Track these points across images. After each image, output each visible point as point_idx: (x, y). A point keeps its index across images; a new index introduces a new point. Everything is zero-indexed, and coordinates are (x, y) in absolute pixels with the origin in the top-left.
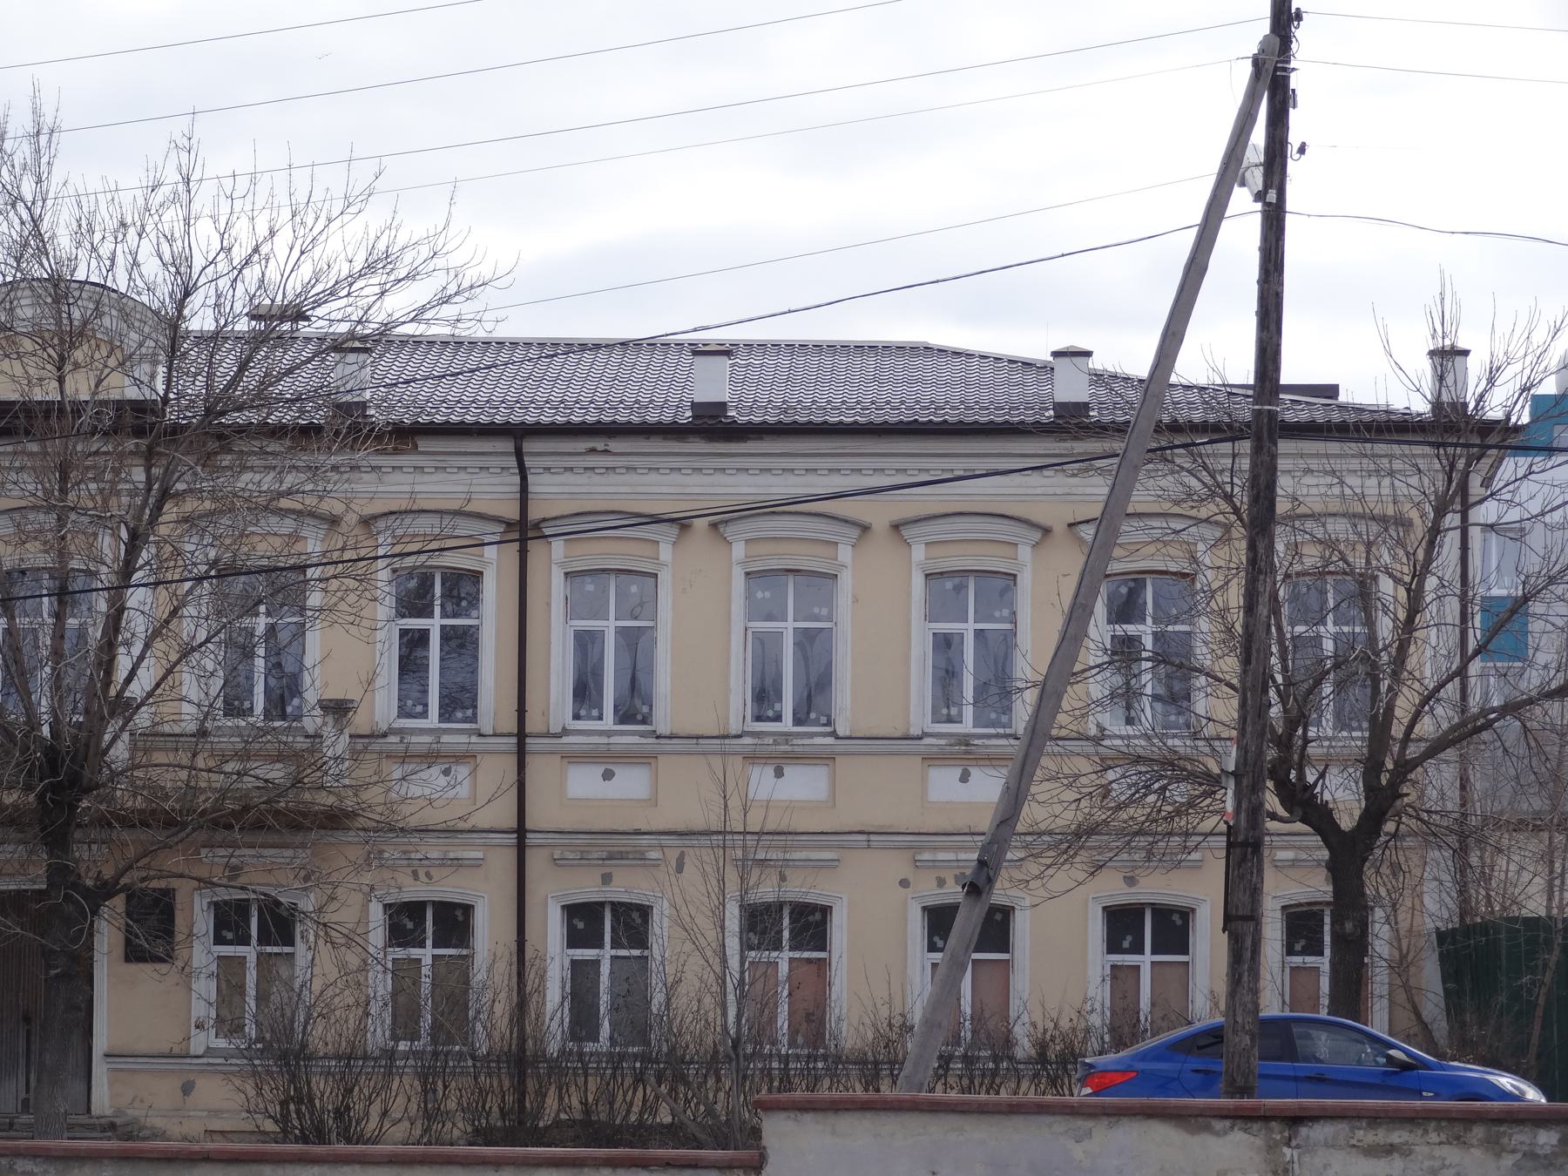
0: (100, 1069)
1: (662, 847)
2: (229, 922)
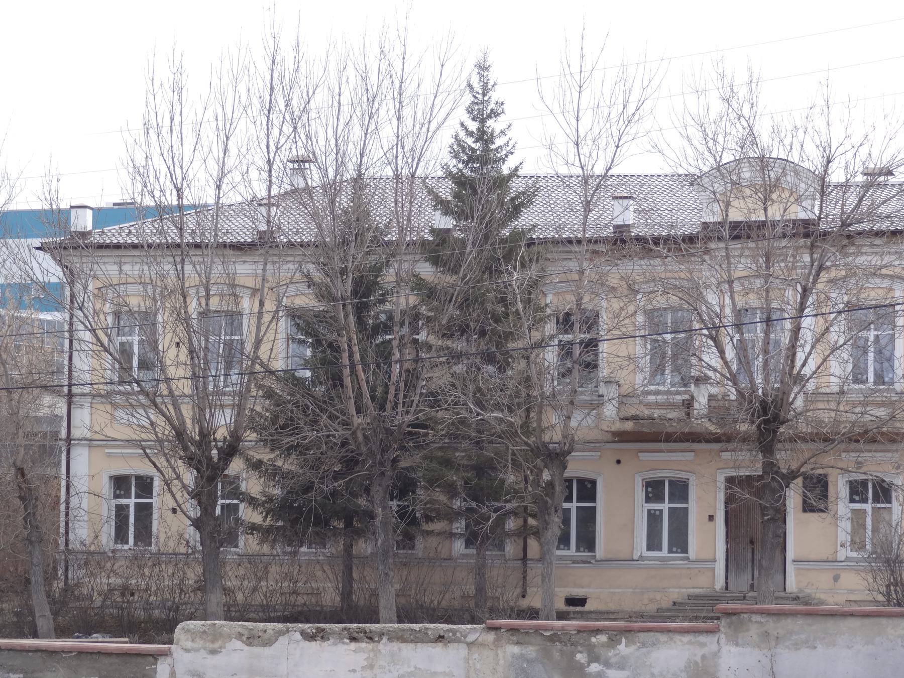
0: (790, 568)
2: (857, 491)
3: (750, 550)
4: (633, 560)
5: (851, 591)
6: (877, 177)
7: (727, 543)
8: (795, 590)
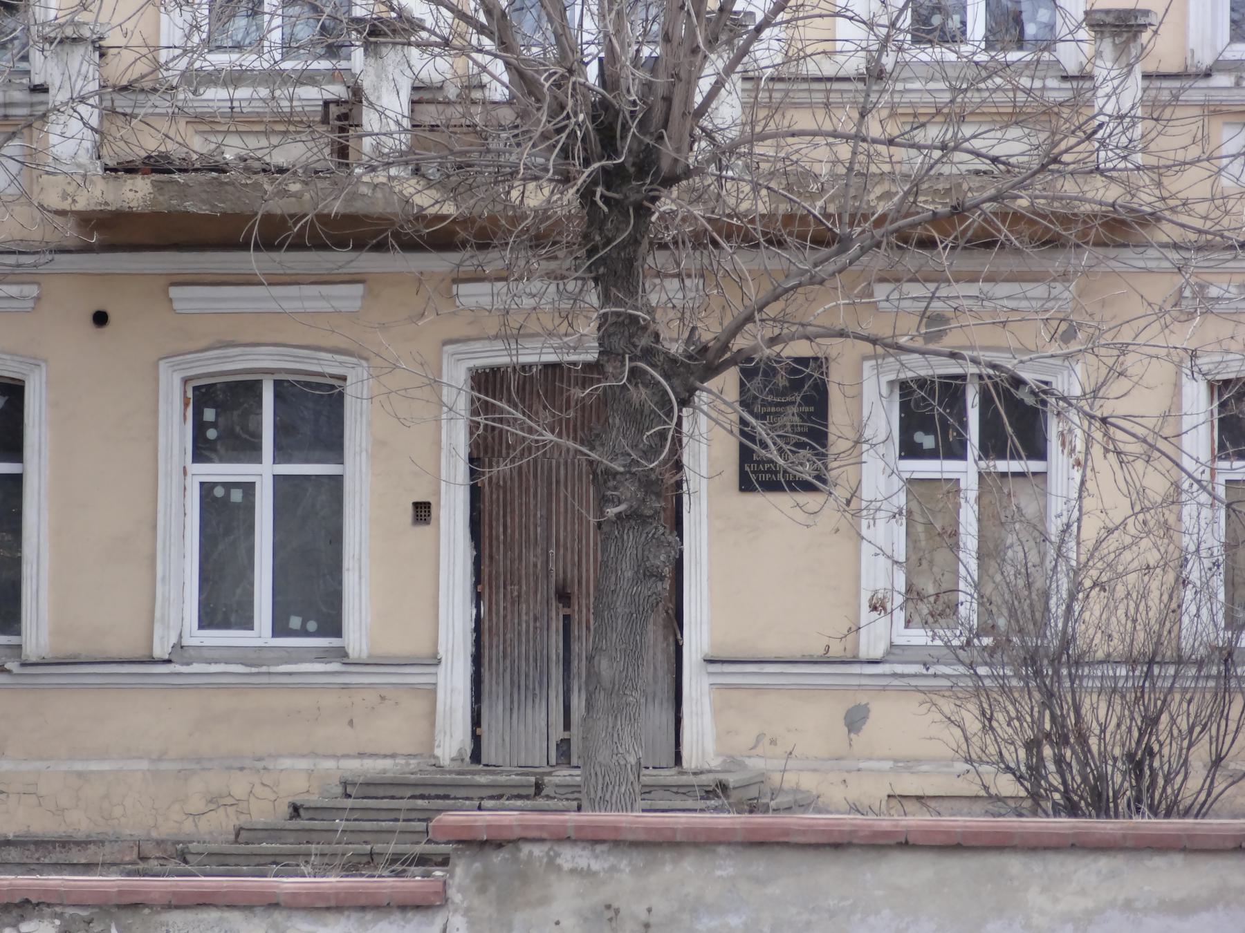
0: (697, 685)
2: (927, 416)
3: (557, 625)
4: (153, 661)
7: (478, 598)
8: (714, 762)
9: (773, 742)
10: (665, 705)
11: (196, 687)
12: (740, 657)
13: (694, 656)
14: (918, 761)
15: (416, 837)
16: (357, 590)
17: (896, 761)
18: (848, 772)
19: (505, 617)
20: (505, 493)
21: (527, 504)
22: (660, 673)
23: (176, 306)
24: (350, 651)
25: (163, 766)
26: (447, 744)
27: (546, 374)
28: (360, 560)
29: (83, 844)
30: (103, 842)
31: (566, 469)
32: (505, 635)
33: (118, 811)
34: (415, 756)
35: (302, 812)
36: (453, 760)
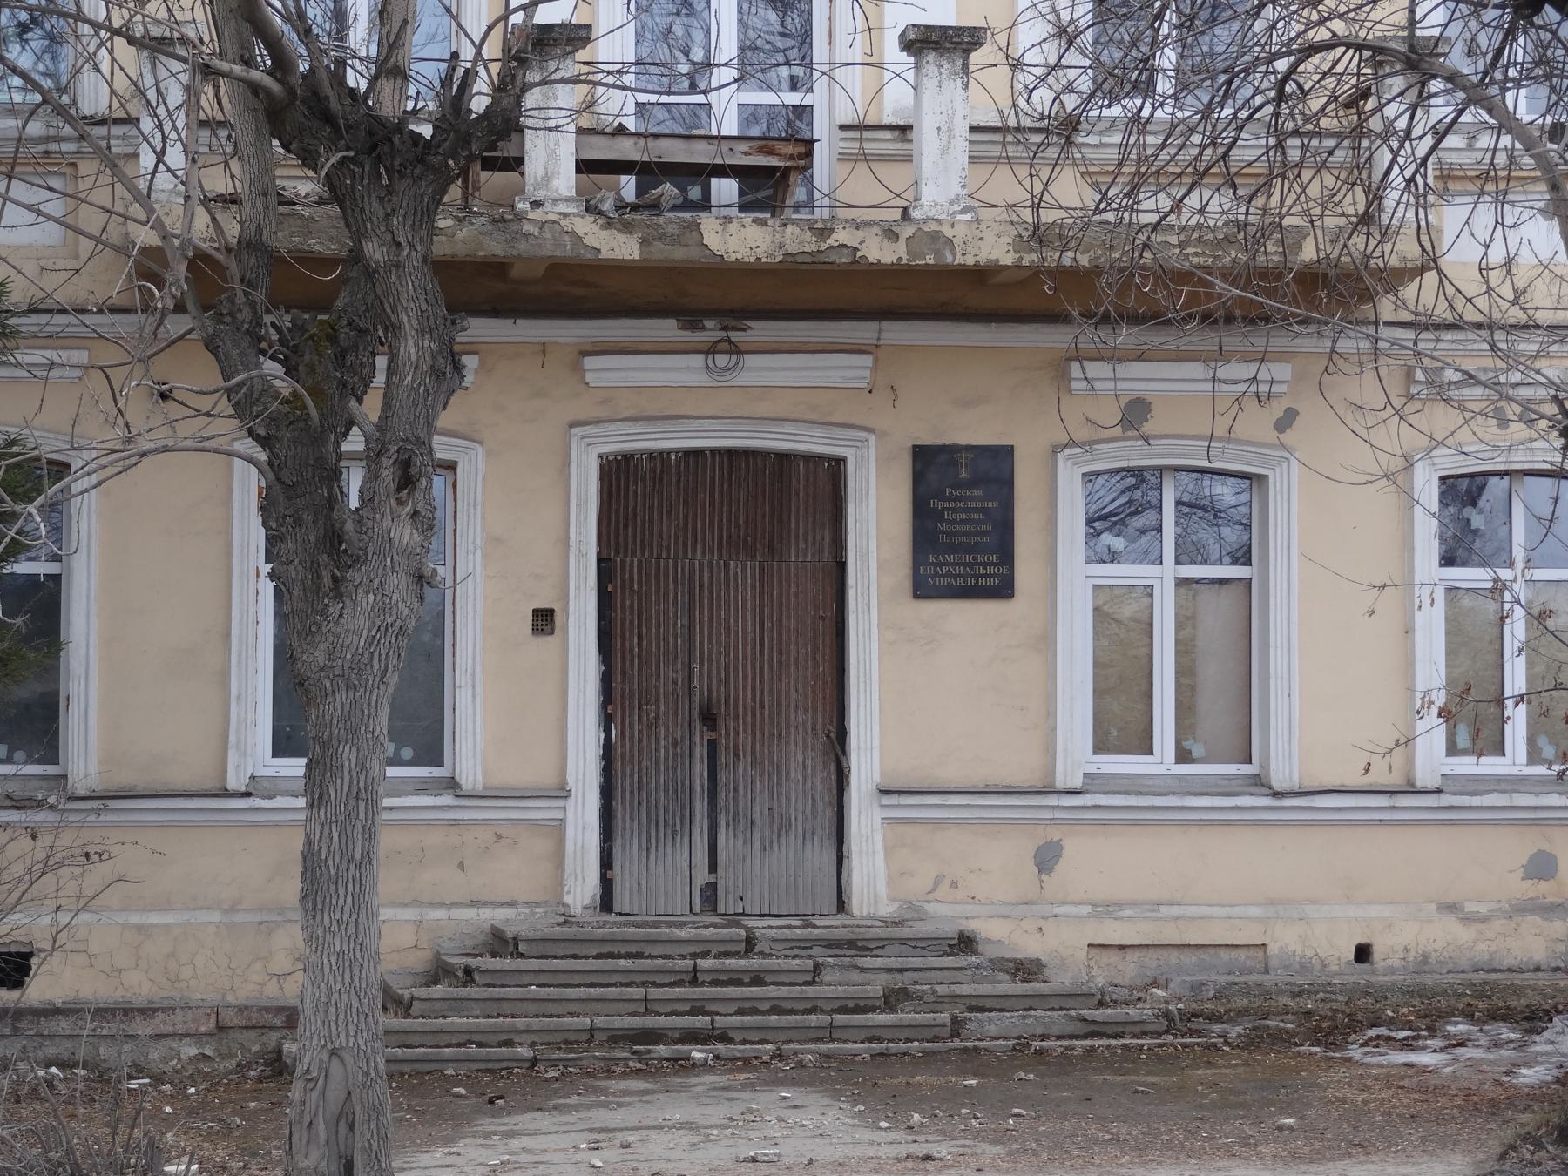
0: (865, 818)
1: (1115, 379)
2: (1122, 512)
3: (700, 751)
4: (226, 794)
5: (1107, 909)
6: (1425, 958)
7: (607, 720)
8: (887, 909)
9: (954, 885)
10: (826, 843)
11: (277, 824)
12: (916, 786)
13: (863, 788)
14: (1120, 905)
15: (632, 1007)
16: (470, 711)
17: (1095, 905)
18: (1045, 918)
19: (640, 741)
20: (640, 600)
21: (666, 613)
22: (820, 806)
23: (589, 377)
24: (463, 782)
25: (240, 918)
26: (579, 889)
27: (687, 463)
28: (473, 675)
29: (148, 1011)
30: (174, 1010)
31: (711, 572)
32: (640, 763)
33: (186, 972)
34: (538, 904)
35: (477, 976)
36: (585, 908)
